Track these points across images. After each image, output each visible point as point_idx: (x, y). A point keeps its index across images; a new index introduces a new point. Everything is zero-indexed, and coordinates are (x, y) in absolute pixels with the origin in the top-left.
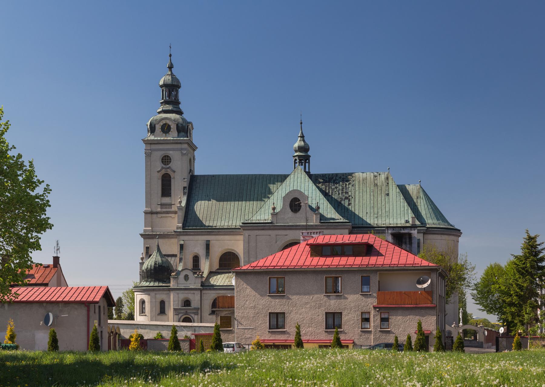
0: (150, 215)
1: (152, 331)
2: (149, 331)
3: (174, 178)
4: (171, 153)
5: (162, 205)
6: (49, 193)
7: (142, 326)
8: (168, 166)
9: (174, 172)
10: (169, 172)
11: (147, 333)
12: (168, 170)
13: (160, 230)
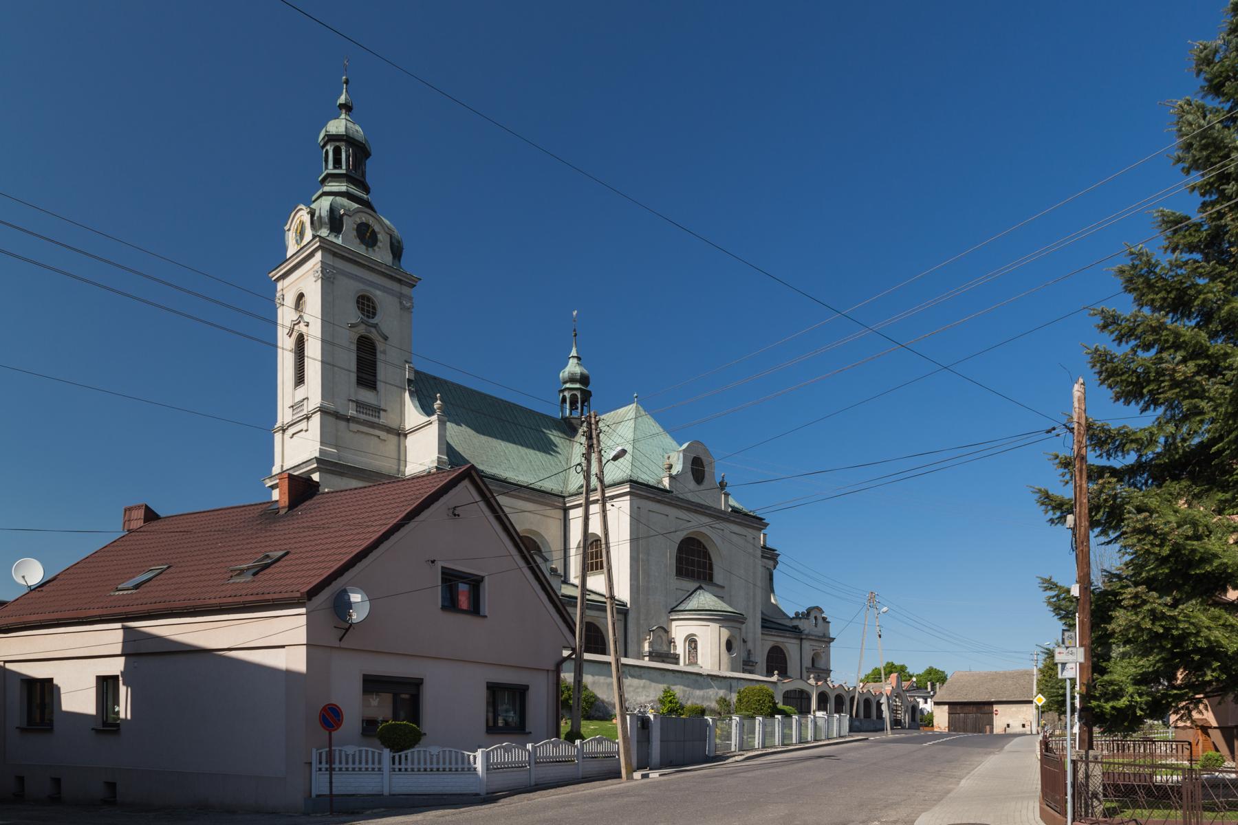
0: (332, 419)
1: (653, 684)
2: (648, 682)
3: (384, 352)
4: (378, 295)
5: (360, 405)
6: (1100, 373)
7: (632, 671)
8: (372, 321)
9: (386, 338)
10: (374, 335)
11: (644, 687)
12: (373, 330)
13: (352, 459)
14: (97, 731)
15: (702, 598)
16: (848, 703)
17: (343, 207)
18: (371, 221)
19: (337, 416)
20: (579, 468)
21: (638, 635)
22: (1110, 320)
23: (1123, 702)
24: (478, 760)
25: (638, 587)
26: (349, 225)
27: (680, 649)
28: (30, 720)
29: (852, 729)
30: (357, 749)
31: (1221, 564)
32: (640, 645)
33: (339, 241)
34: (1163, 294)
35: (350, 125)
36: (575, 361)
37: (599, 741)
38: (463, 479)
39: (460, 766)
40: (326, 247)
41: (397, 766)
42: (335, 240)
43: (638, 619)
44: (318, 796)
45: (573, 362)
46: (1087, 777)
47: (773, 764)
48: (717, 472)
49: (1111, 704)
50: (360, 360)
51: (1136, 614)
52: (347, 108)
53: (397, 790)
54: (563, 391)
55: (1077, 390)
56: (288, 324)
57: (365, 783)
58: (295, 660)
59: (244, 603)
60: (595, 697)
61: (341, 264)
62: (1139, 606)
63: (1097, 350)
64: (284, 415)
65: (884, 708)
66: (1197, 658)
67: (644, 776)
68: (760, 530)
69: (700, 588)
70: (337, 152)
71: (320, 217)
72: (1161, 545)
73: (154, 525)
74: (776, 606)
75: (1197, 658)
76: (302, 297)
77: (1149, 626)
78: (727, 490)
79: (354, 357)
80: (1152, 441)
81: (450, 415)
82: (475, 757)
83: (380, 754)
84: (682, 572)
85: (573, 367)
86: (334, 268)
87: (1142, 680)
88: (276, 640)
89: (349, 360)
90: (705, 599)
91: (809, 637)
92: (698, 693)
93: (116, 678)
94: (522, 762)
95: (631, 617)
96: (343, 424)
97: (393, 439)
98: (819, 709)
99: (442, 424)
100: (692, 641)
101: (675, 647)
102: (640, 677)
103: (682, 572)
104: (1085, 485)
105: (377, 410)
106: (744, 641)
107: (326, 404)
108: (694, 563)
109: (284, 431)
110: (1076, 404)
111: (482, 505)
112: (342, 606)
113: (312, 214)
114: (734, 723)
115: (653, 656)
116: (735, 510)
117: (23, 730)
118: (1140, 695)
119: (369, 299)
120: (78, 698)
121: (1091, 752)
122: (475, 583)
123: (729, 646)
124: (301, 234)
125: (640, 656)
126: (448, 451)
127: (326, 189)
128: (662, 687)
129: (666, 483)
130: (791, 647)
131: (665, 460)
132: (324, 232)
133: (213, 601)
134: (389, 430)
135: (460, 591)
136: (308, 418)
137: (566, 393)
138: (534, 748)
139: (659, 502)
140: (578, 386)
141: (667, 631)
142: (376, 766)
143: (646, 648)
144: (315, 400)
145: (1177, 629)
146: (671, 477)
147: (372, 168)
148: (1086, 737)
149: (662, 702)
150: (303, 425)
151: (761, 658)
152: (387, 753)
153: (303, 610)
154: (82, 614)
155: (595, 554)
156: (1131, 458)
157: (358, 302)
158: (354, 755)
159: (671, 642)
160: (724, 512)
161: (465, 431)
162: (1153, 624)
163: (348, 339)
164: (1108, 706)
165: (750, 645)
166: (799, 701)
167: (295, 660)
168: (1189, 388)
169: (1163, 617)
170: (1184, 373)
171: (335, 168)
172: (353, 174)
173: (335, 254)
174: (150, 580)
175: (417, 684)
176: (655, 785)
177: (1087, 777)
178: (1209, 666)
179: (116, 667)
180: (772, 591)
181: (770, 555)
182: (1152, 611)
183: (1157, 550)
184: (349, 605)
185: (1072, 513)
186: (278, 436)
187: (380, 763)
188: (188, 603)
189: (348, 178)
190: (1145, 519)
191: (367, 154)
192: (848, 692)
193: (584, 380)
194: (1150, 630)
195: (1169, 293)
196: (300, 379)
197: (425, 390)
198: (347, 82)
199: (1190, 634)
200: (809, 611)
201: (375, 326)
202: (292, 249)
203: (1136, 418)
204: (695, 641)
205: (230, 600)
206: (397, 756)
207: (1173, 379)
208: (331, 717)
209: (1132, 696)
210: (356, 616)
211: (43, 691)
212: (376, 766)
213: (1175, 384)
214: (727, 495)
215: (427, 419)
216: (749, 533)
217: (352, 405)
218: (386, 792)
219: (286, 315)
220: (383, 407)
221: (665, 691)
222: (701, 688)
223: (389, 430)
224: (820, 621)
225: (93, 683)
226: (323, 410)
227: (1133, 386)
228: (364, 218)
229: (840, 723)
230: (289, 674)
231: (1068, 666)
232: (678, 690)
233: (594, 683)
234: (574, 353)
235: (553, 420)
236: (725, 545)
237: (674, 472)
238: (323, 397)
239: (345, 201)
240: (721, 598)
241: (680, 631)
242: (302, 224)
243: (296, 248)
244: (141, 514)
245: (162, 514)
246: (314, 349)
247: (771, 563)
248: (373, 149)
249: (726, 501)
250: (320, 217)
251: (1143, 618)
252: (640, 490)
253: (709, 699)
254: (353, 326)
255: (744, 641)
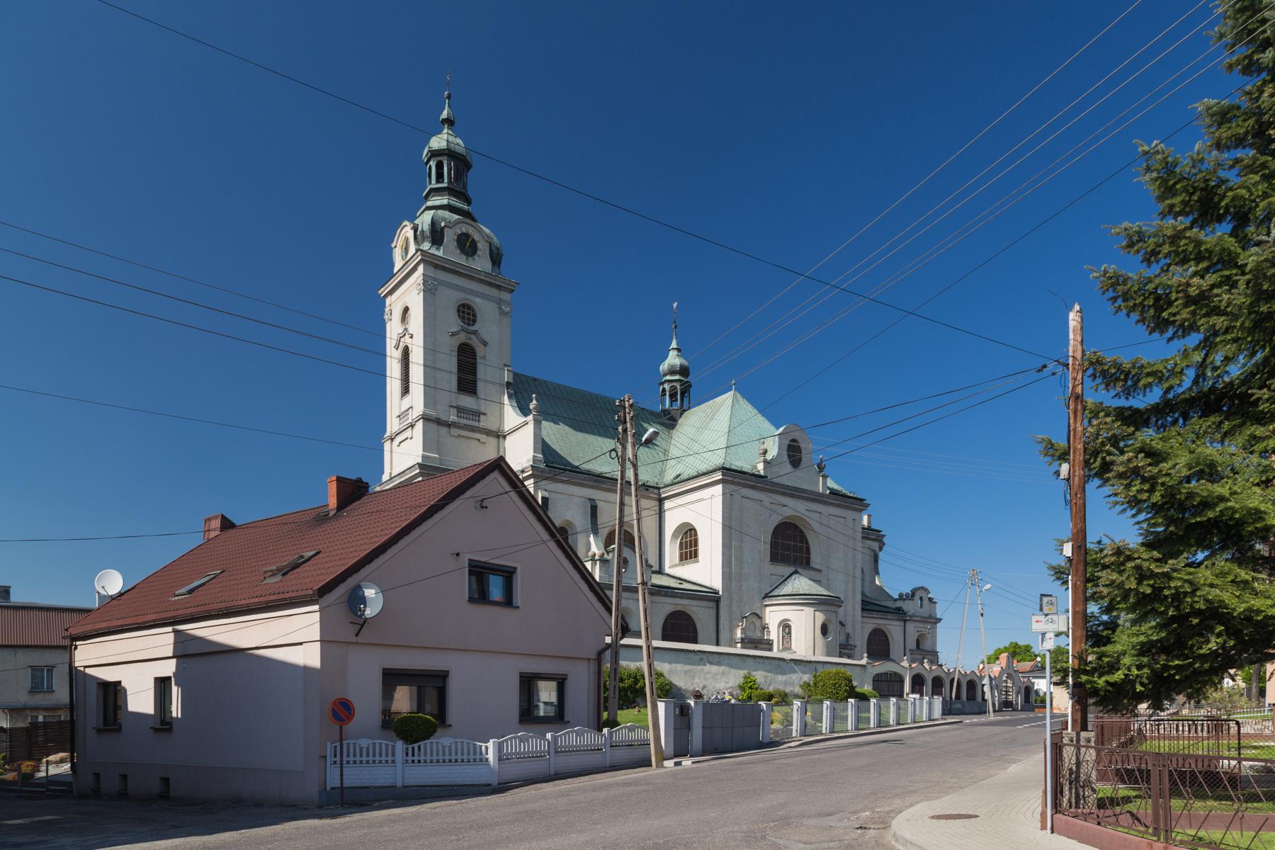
0: (434, 426)
3: (484, 358)
4: (478, 303)
5: (461, 410)
7: (711, 657)
9: (485, 344)
10: (474, 342)
11: (723, 673)
12: (473, 337)
14: (156, 730)
15: (797, 582)
16: (948, 685)
17: (444, 219)
18: (471, 231)
19: (439, 422)
20: (613, 454)
21: (731, 622)
22: (1135, 238)
23: (1118, 676)
24: (490, 750)
25: (730, 574)
26: (450, 237)
27: (774, 634)
28: (106, 722)
29: (947, 711)
30: (452, 740)
31: (1226, 509)
32: (732, 630)
33: (440, 253)
34: (1184, 196)
35: (451, 139)
36: (675, 352)
37: (631, 729)
38: (492, 471)
39: (472, 757)
40: (427, 260)
41: (410, 758)
42: (436, 253)
43: (730, 606)
44: (333, 789)
45: (673, 354)
46: (1078, 764)
47: (806, 753)
48: (811, 455)
49: (1103, 679)
50: (473, 371)
51: (1121, 572)
52: (449, 122)
53: (409, 782)
54: (662, 383)
55: (1073, 318)
56: (395, 337)
57: (379, 776)
58: (310, 656)
59: (267, 602)
60: (671, 684)
61: (441, 275)
62: (1123, 564)
63: (1105, 272)
64: (393, 425)
65: (987, 689)
66: (1195, 621)
67: (677, 764)
68: (861, 511)
69: (796, 572)
70: (439, 166)
71: (422, 231)
72: (1152, 490)
73: (231, 532)
74: (880, 589)
75: (1195, 621)
76: (407, 310)
77: (1133, 586)
78: (825, 472)
79: (455, 360)
80: (1177, 373)
81: (545, 414)
82: (487, 748)
83: (393, 747)
84: (776, 558)
85: (673, 359)
86: (435, 279)
87: (1145, 649)
88: (292, 637)
89: (452, 364)
90: (800, 584)
91: (913, 619)
92: (781, 678)
93: (169, 678)
94: (541, 752)
95: (723, 604)
96: (444, 430)
97: (492, 441)
98: (913, 691)
99: (537, 423)
100: (786, 627)
101: (769, 632)
102: (719, 664)
103: (776, 558)
104: (1080, 429)
105: (478, 414)
106: (842, 624)
107: (428, 412)
108: (790, 547)
109: (392, 440)
110: (1071, 336)
111: (513, 495)
112: (356, 600)
113: (415, 229)
114: (795, 707)
115: (746, 642)
116: (834, 493)
117: (99, 731)
118: (1139, 667)
119: (469, 307)
120: (141, 701)
121: (1083, 734)
122: (508, 575)
123: (824, 630)
124: (406, 250)
125: (732, 643)
126: (543, 447)
127: (429, 204)
128: (742, 673)
129: (761, 467)
130: (893, 629)
131: (760, 444)
132: (426, 246)
133: (243, 602)
134: (489, 433)
135: (488, 581)
136: (412, 426)
137: (667, 386)
138: (555, 738)
139: (753, 487)
140: (677, 377)
141: (760, 617)
142: (390, 758)
143: (739, 634)
144: (419, 408)
145: (1170, 588)
146: (765, 462)
147: (474, 181)
148: (1079, 717)
149: (742, 688)
150: (408, 434)
151: (860, 640)
152: (400, 745)
153: (316, 607)
154: (141, 619)
155: (689, 545)
156: (1154, 396)
157: (458, 311)
158: (368, 748)
159: (765, 628)
160: (823, 495)
161: (563, 428)
162: (1140, 583)
163: (449, 347)
164: (1101, 682)
165: (849, 629)
166: (888, 686)
167: (310, 656)
168: (1201, 301)
169: (1153, 575)
170: (1199, 287)
171: (438, 182)
172: (455, 186)
173: (436, 266)
174: (203, 584)
175: (443, 676)
176: (686, 771)
177: (1078, 764)
178: (1211, 630)
179: (168, 668)
180: (877, 573)
181: (873, 535)
182: (1138, 568)
183: (1145, 496)
184: (363, 600)
185: (1067, 460)
186: (387, 446)
187: (393, 755)
188: (223, 605)
189: (450, 191)
190: (1129, 460)
191: (468, 166)
192: (948, 673)
193: (684, 371)
194: (1136, 590)
195: (1191, 194)
196: (406, 390)
197: (521, 390)
198: (449, 97)
199: (1185, 593)
200: (914, 593)
201: (475, 333)
202: (398, 264)
203: (1158, 350)
204: (789, 627)
205: (257, 600)
206: (410, 747)
207: (1187, 296)
208: (343, 711)
209: (1129, 670)
210: (369, 612)
211: (113, 692)
212: (390, 758)
213: (1189, 301)
214: (825, 477)
215: (524, 419)
216: (850, 514)
217: (454, 411)
218: (399, 784)
219: (393, 328)
220: (483, 410)
221: (745, 677)
222: (784, 673)
223: (489, 433)
224: (926, 602)
225: (151, 684)
226: (425, 418)
227: (1156, 310)
228: (464, 229)
229: (926, 706)
230: (306, 669)
231: (1047, 636)
232: (760, 676)
233: (671, 671)
234: (674, 345)
235: (652, 413)
236: (820, 524)
237: (769, 457)
238: (426, 404)
239: (446, 214)
240: (818, 582)
241: (773, 616)
242: (407, 240)
243: (402, 263)
244: (216, 523)
245: (237, 523)
246: (417, 357)
247: (875, 545)
248: (474, 159)
249: (825, 483)
250: (422, 231)
251: (1128, 578)
252: (732, 477)
253: (793, 684)
254: (453, 334)
255: (842, 624)
